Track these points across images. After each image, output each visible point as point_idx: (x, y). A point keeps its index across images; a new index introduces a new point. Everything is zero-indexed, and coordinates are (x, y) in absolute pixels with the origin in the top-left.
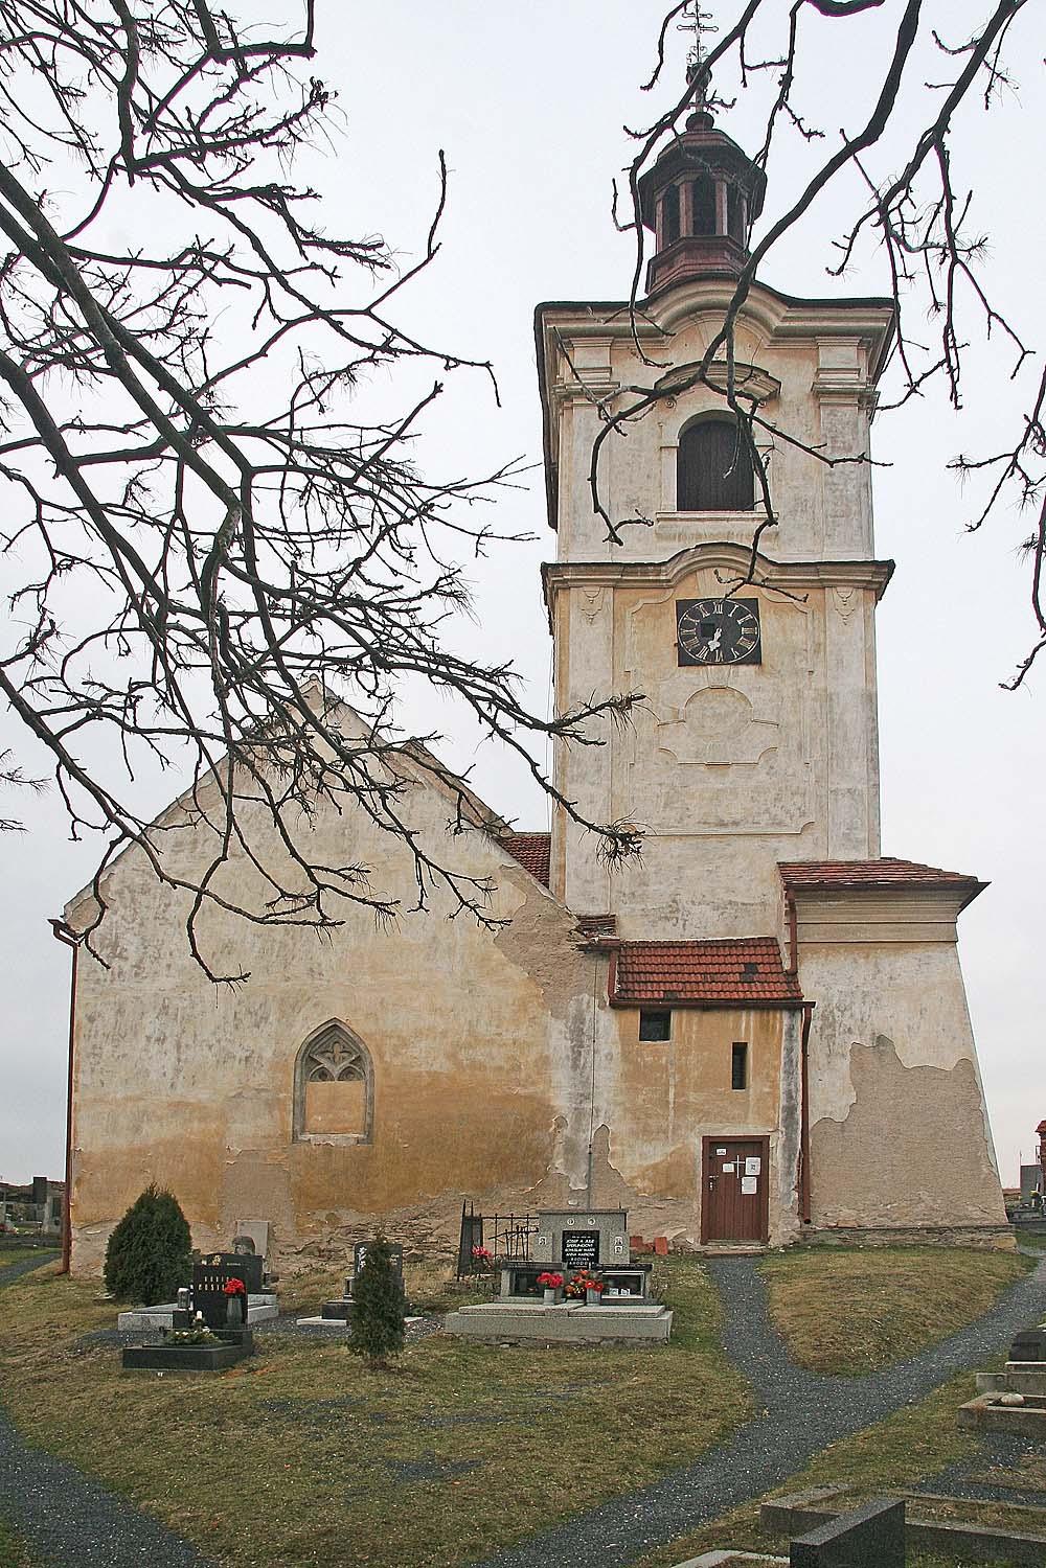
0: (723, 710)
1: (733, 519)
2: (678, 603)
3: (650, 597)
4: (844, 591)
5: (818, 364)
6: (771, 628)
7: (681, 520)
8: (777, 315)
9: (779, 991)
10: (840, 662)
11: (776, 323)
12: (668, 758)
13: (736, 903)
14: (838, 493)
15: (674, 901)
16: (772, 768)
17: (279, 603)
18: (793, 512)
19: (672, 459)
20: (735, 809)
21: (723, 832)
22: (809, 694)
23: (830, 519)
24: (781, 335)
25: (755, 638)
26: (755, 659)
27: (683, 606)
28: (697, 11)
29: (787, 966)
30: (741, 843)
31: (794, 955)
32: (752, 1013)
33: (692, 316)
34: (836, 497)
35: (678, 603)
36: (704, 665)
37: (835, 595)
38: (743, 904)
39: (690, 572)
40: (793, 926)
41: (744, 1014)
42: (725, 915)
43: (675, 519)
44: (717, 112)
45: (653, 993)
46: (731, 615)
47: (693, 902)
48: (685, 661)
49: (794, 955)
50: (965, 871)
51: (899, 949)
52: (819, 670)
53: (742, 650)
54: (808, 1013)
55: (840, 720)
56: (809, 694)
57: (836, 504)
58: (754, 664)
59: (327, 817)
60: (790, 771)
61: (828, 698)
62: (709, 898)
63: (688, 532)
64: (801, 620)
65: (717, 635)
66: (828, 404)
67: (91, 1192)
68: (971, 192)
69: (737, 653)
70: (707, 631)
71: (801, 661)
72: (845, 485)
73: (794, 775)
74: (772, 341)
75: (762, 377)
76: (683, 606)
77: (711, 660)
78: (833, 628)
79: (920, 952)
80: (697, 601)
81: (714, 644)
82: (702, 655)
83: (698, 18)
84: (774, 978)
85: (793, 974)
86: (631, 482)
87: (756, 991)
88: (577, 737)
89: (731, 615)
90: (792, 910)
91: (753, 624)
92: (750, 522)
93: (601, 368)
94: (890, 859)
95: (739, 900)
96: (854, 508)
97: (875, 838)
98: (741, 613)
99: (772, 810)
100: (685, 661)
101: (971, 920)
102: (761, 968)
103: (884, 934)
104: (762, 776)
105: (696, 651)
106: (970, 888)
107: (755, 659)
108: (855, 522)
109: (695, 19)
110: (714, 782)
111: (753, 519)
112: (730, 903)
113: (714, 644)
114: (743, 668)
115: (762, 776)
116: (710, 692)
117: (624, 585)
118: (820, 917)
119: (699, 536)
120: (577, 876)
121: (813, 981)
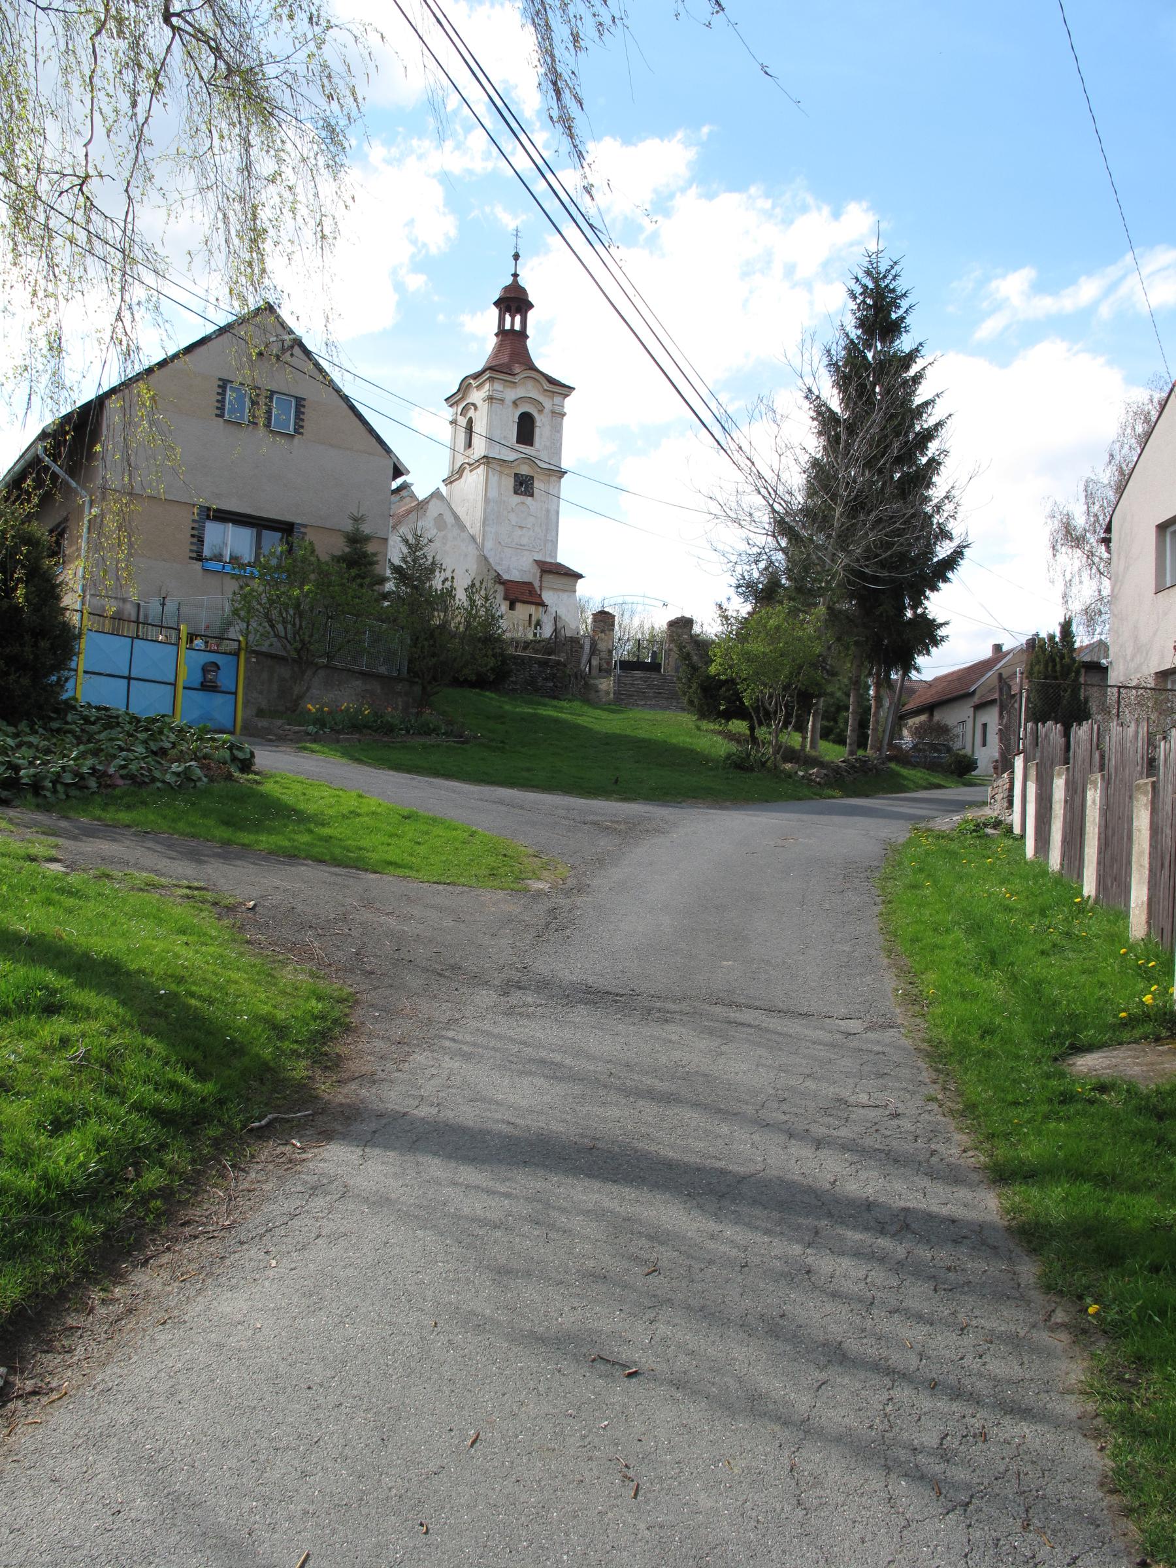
20: (524, 541)
21: (521, 548)
26: (532, 495)
27: (516, 475)
30: (525, 552)
40: (541, 581)
44: (857, 280)
45: (512, 597)
48: (516, 493)
50: (580, 572)
67: (713, 1062)
68: (593, 199)
70: (521, 484)
76: (516, 475)
77: (521, 494)
85: (540, 595)
88: (91, 78)
90: (541, 577)
97: (556, 557)
101: (580, 581)
103: (561, 587)
106: (580, 576)
107: (532, 495)
110: (519, 532)
121: (547, 597)
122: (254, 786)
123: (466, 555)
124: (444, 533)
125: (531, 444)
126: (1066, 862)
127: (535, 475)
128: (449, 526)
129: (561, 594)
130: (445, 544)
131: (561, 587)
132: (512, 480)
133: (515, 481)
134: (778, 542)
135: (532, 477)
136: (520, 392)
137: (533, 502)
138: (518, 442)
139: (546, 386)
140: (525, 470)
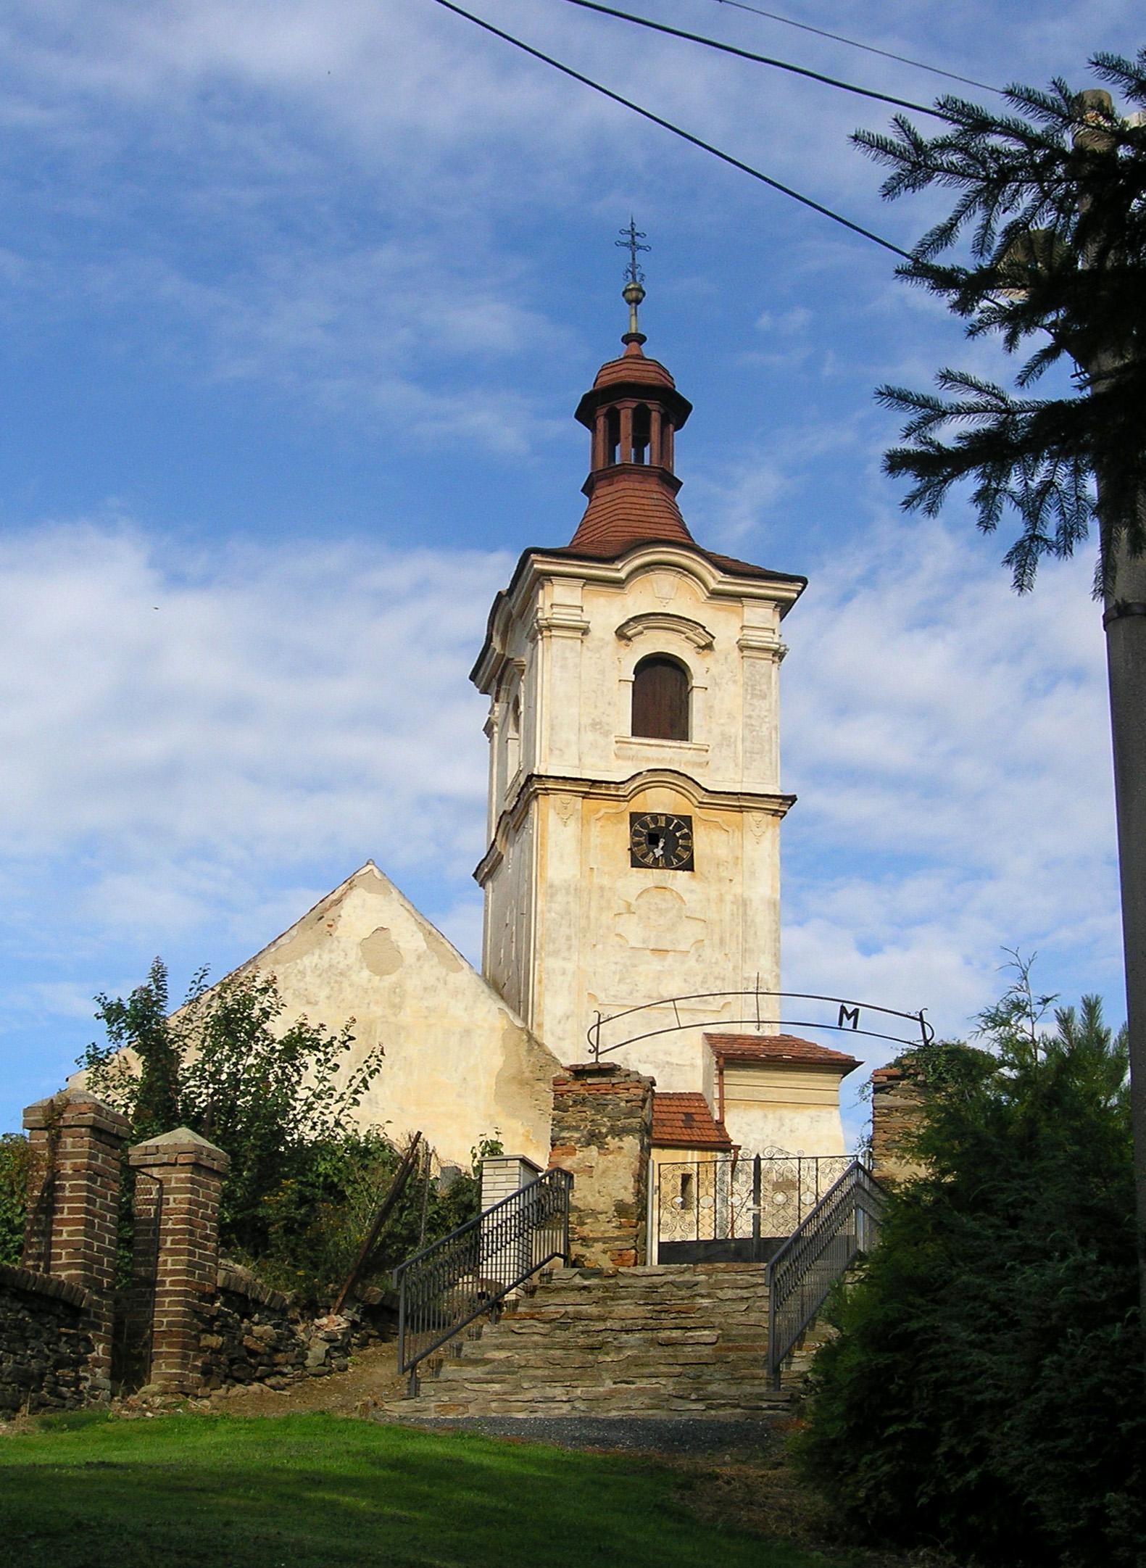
0: (664, 905)
1: (674, 747)
2: (632, 815)
3: (609, 807)
4: (758, 815)
5: (743, 620)
6: (704, 842)
7: (634, 743)
8: (714, 578)
9: (713, 1137)
10: (753, 873)
11: (713, 585)
12: (622, 942)
13: (672, 1064)
14: (754, 733)
15: (626, 1059)
16: (700, 956)
17: (1105, 1501)
18: (720, 745)
19: (628, 691)
22: (729, 898)
23: (748, 755)
24: (716, 594)
25: (689, 849)
26: (689, 866)
27: (635, 817)
28: (633, 229)
29: (717, 1117)
31: (722, 1108)
32: (696, 1152)
33: (647, 569)
34: (753, 736)
35: (632, 815)
36: (651, 868)
37: (750, 817)
38: (677, 1065)
39: (641, 789)
40: (721, 1085)
41: (690, 1152)
42: (664, 1073)
43: (630, 743)
46: (671, 828)
47: (640, 1061)
48: (636, 863)
49: (722, 1108)
51: (798, 1108)
52: (737, 879)
53: (680, 858)
54: (736, 1154)
55: (752, 921)
56: (729, 898)
57: (753, 742)
58: (688, 870)
59: (665, 1214)
60: (714, 960)
61: (744, 903)
62: (651, 1059)
63: (639, 755)
64: (724, 835)
65: (661, 845)
66: (749, 657)
69: (675, 861)
70: (653, 840)
71: (723, 871)
72: (761, 727)
73: (716, 963)
74: (708, 598)
75: (701, 630)
76: (635, 817)
77: (655, 865)
78: (749, 845)
79: (812, 1112)
80: (646, 814)
81: (659, 852)
82: (649, 860)
83: (633, 237)
84: (706, 1125)
85: (721, 1123)
86: (596, 707)
87: (696, 1135)
89: (671, 828)
91: (688, 837)
92: (687, 751)
93: (576, 606)
94: (788, 1036)
95: (674, 1061)
96: (767, 747)
98: (678, 827)
99: (860, 1158)
100: (636, 863)
102: (697, 1117)
103: (787, 1095)
104: (691, 962)
105: (644, 856)
107: (689, 866)
108: (767, 760)
109: (630, 236)
110: (656, 965)
111: (690, 749)
112: (668, 1063)
113: (659, 852)
114: (680, 872)
115: (691, 962)
116: (654, 892)
117: (591, 796)
118: (742, 1082)
119: (648, 759)
120: (552, 1034)
122: (276, 1475)
123: (468, 1032)
124: (393, 978)
125: (684, 736)
126: (532, 758)
127: (696, 813)
128: (410, 959)
129: (787, 1113)
130: (397, 1007)
131: (787, 1095)
132: (625, 828)
133: (634, 833)
134: (511, 1288)
135: (687, 820)
136: (639, 599)
137: (694, 884)
138: (634, 734)
139: (715, 579)
140: (660, 802)
